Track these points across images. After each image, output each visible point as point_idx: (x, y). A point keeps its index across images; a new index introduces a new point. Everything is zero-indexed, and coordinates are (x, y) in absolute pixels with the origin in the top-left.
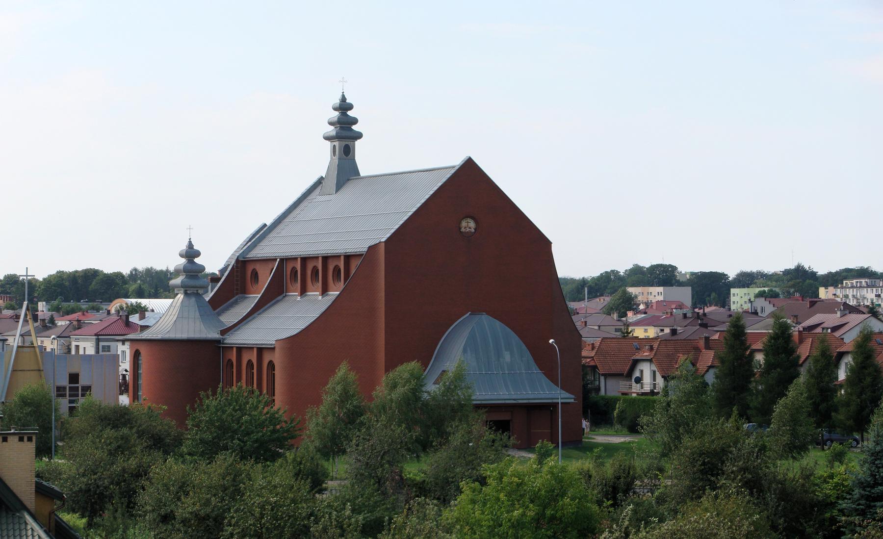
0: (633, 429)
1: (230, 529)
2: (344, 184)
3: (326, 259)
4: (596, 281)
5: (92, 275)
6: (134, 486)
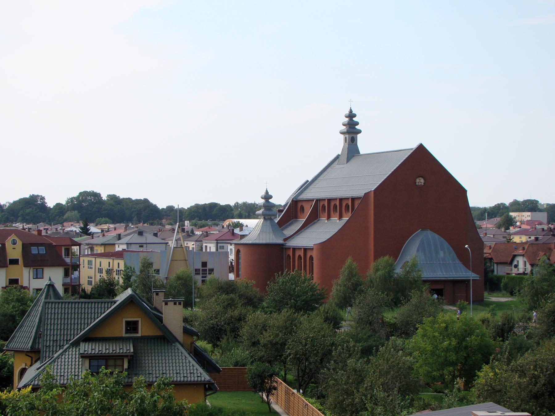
0: (512, 294)
1: (289, 351)
2: (351, 158)
3: (341, 200)
4: (493, 210)
5: (214, 206)
6: (237, 325)
